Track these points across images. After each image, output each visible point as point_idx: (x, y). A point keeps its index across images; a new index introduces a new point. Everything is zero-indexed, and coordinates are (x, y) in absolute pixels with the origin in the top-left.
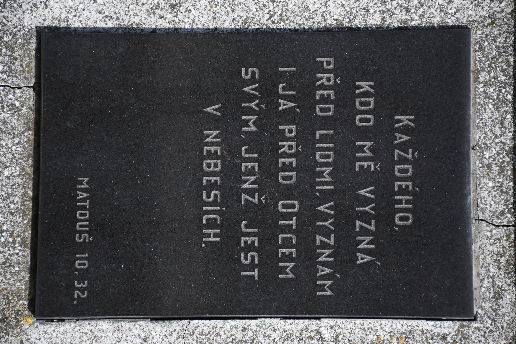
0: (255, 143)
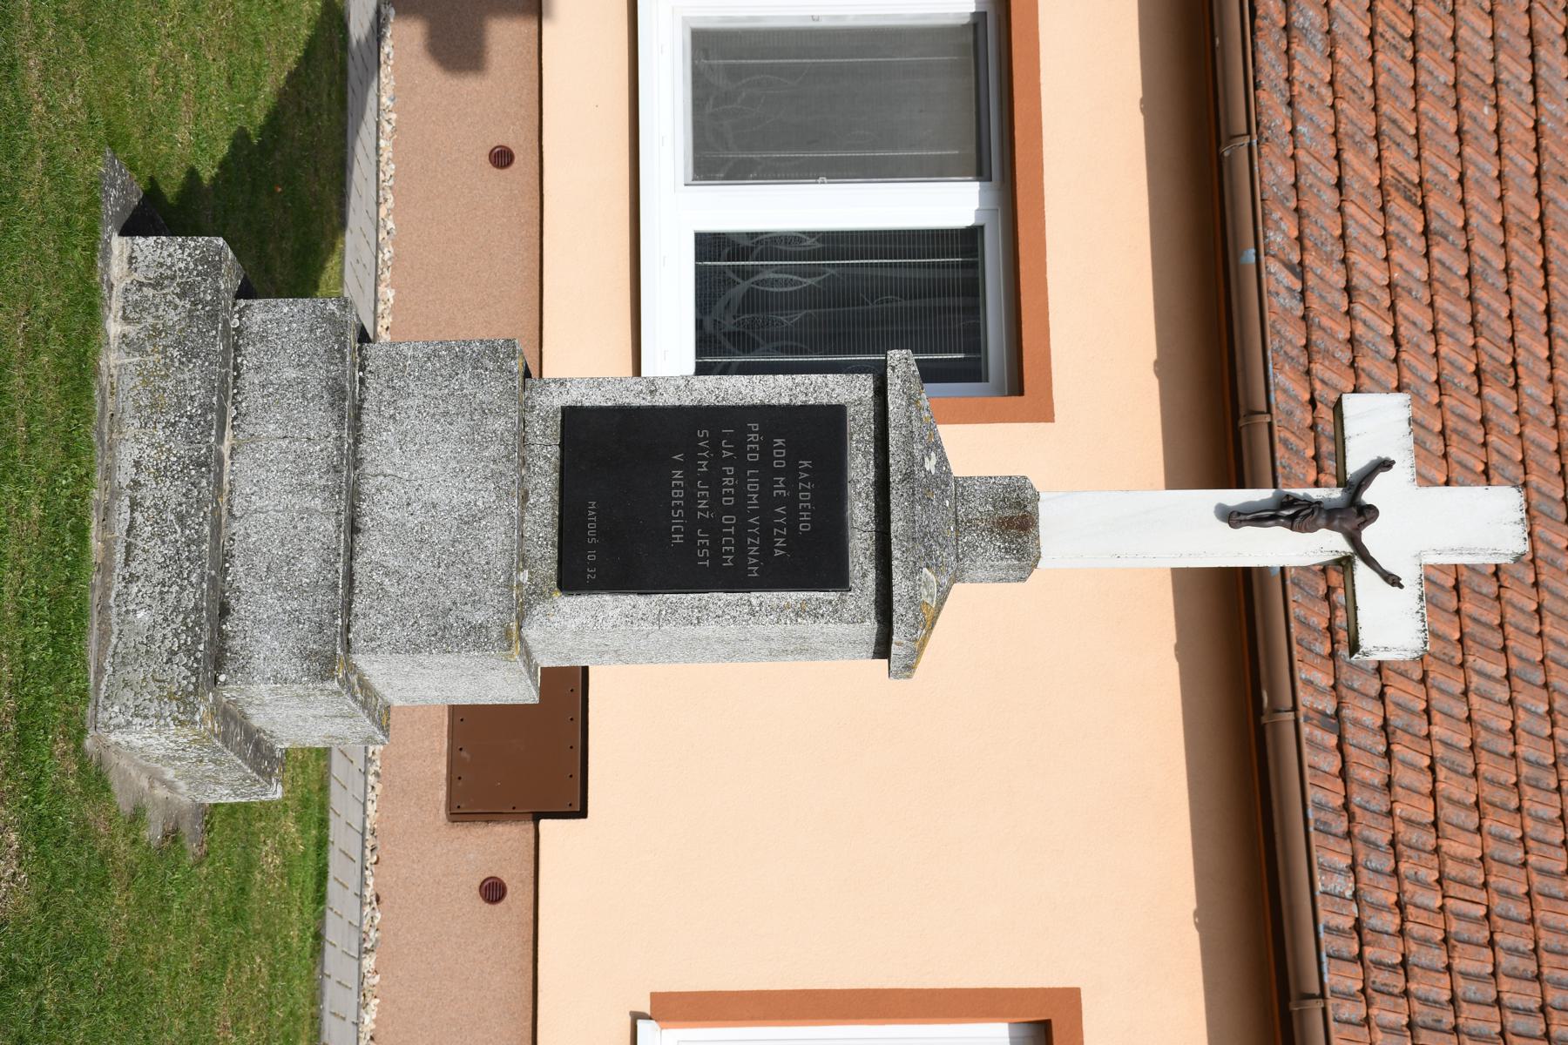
0: (706, 478)
